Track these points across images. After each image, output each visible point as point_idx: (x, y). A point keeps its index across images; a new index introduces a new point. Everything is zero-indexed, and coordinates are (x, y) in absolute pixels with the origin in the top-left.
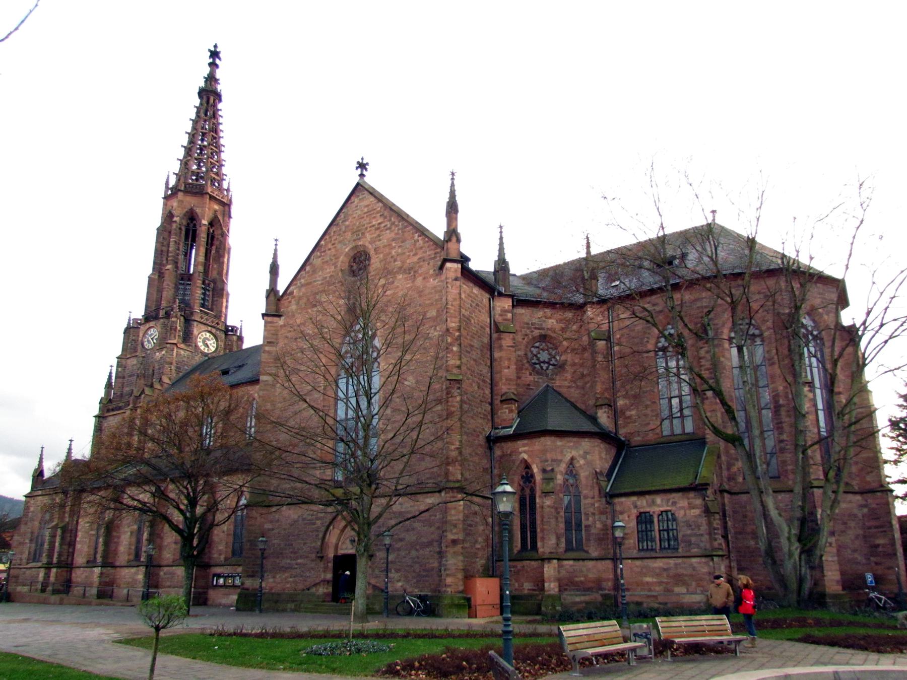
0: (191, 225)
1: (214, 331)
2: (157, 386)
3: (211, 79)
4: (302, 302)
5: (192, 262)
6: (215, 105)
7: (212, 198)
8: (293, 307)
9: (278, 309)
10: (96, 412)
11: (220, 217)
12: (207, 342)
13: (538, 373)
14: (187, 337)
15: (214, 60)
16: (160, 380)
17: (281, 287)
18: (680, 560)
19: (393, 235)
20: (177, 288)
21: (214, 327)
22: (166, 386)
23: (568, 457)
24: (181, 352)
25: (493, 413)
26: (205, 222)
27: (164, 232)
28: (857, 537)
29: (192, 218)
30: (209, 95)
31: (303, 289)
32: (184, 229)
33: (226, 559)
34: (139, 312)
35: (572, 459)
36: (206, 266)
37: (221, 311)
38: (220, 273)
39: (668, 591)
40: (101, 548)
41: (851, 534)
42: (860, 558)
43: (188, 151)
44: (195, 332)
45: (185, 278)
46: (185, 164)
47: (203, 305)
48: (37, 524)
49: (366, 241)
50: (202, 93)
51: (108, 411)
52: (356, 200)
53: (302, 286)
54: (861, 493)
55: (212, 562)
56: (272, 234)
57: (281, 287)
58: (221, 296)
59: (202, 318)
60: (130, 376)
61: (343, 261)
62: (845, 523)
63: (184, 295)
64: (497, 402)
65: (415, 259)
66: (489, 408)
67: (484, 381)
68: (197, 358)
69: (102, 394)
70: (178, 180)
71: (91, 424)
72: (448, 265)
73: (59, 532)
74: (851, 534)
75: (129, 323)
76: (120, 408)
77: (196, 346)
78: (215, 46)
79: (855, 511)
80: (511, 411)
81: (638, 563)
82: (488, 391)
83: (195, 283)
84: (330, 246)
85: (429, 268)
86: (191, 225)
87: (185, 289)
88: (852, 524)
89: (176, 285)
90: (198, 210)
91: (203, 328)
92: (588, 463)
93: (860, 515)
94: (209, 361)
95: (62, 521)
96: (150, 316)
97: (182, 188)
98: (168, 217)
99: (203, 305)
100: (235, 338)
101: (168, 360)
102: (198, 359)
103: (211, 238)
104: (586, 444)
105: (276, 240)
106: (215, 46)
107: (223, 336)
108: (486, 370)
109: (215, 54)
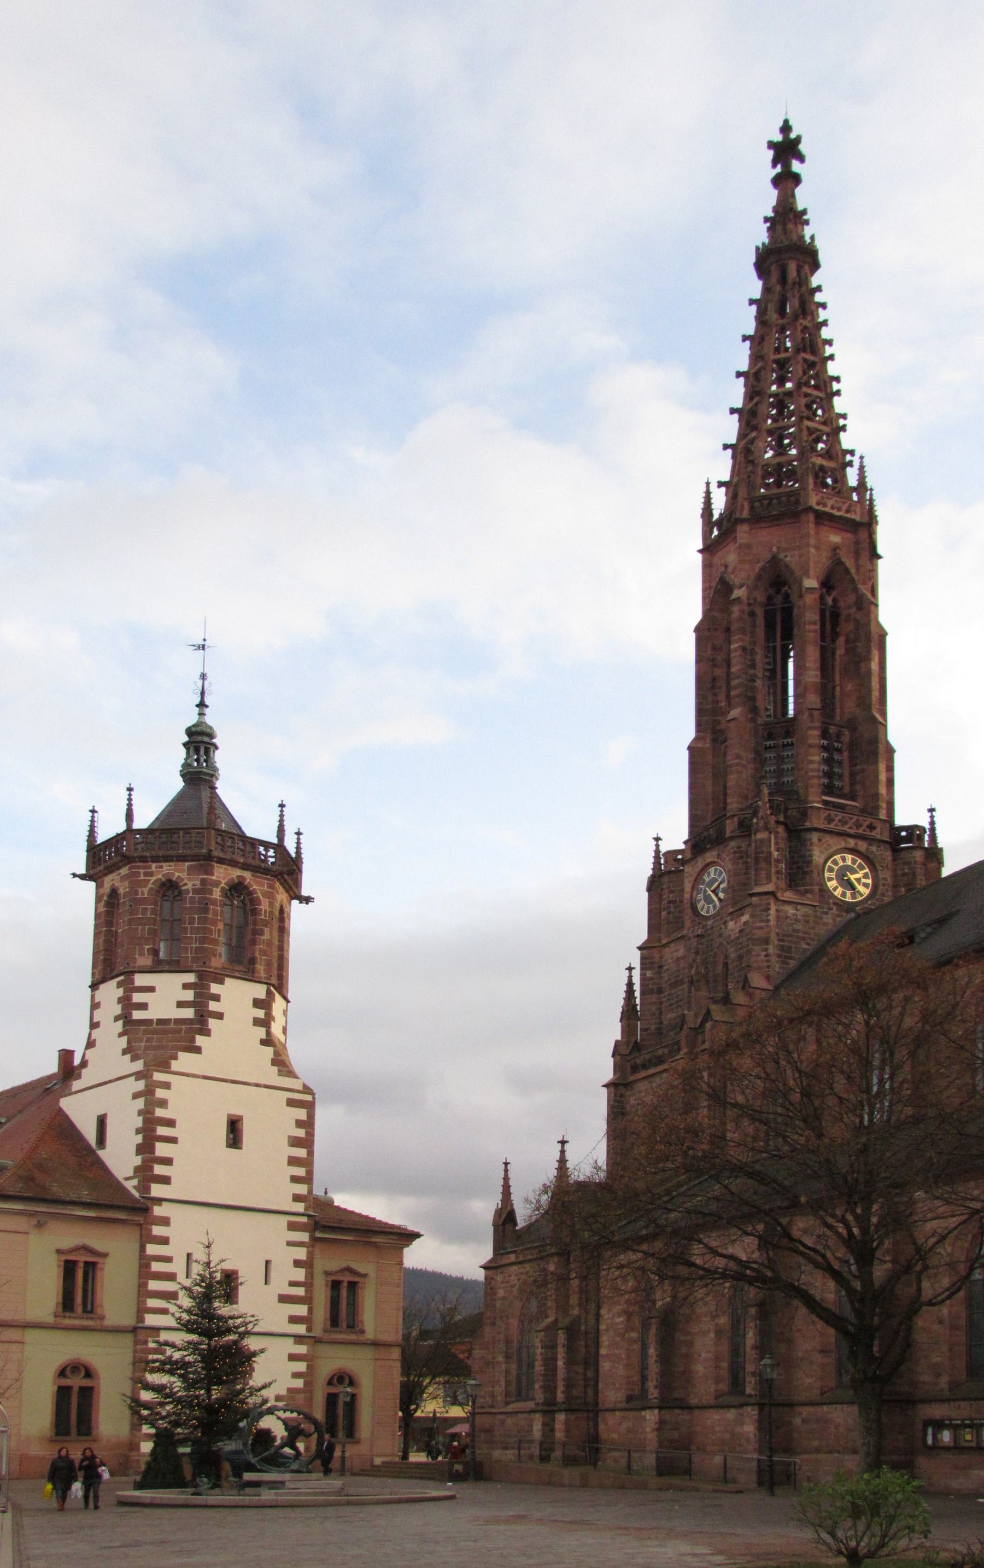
0: (779, 599)
1: (862, 846)
2: (739, 998)
3: (786, 217)
6: (803, 281)
10: (608, 1074)
11: (849, 563)
12: (849, 878)
14: (800, 873)
15: (787, 166)
21: (863, 838)
24: (790, 910)
29: (777, 580)
30: (787, 260)
32: (759, 612)
33: (954, 1385)
34: (676, 836)
37: (876, 796)
40: (654, 1368)
44: (817, 856)
45: (779, 731)
46: (742, 452)
47: (829, 789)
48: (514, 1322)
50: (766, 261)
51: (635, 1069)
60: (675, 985)
68: (828, 919)
69: (615, 1032)
73: (561, 1337)
77: (824, 892)
87: (780, 759)
89: (757, 753)
90: (791, 559)
94: (858, 919)
99: (829, 789)
102: (831, 921)
103: (831, 620)
107: (888, 855)
109: (786, 150)
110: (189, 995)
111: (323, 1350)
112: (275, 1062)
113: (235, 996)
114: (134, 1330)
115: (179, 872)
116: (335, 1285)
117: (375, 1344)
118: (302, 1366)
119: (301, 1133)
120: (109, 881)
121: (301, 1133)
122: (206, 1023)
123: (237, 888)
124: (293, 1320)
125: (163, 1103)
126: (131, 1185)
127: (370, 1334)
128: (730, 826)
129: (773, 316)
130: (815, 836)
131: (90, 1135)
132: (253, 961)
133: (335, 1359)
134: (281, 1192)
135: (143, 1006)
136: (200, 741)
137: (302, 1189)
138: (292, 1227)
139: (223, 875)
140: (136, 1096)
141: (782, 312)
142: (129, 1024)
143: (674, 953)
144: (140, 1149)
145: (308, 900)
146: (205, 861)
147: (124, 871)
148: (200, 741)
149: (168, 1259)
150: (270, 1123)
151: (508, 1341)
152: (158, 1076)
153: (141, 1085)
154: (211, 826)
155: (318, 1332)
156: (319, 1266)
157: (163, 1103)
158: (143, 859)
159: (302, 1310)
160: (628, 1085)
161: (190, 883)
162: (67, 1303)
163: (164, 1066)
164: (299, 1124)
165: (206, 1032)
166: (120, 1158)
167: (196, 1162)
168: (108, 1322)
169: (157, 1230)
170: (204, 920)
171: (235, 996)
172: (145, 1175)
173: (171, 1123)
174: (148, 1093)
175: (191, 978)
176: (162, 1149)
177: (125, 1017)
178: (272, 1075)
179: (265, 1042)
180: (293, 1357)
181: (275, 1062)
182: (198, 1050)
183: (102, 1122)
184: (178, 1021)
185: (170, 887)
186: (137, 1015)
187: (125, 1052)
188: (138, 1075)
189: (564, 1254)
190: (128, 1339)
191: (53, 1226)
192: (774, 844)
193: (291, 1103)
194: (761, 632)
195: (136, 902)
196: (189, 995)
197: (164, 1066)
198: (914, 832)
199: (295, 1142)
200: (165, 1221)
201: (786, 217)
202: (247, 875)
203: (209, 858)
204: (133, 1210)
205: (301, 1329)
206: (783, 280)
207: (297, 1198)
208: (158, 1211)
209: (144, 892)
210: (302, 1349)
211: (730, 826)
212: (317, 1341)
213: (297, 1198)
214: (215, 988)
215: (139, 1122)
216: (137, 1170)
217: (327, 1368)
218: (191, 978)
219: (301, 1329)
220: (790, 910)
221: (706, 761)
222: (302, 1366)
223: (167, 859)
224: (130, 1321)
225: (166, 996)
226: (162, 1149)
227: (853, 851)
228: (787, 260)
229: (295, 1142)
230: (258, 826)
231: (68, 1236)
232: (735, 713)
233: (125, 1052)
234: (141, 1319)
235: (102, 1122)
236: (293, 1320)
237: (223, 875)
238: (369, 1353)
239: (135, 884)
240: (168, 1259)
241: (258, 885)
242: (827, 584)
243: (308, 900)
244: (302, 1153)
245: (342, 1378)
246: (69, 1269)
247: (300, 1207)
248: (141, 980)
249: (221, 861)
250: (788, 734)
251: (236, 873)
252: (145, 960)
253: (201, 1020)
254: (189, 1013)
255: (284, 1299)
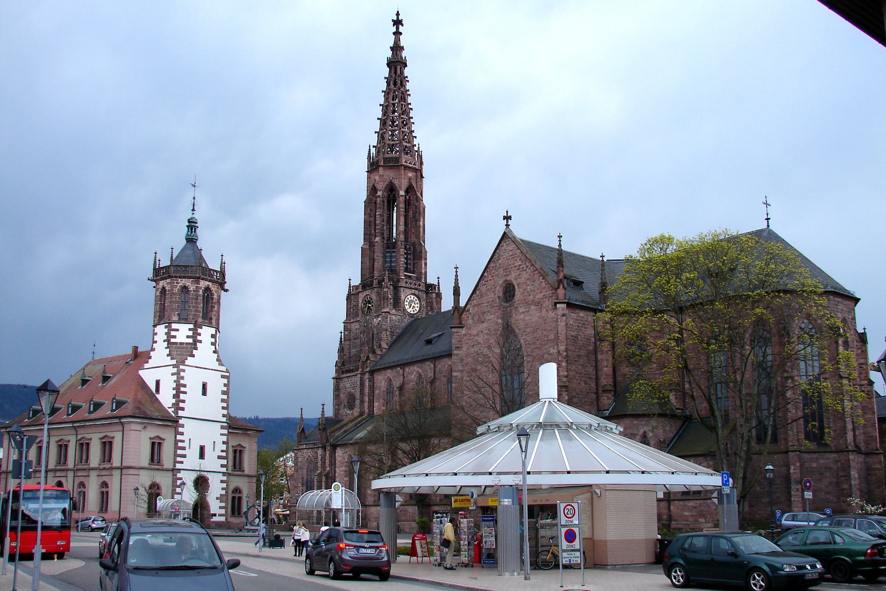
0: (392, 196)
1: (417, 292)
2: (378, 352)
3: (397, 48)
4: (476, 318)
5: (395, 223)
6: (402, 73)
7: (406, 167)
8: (470, 321)
9: (460, 323)
10: (334, 374)
11: (414, 184)
12: (412, 305)
13: (633, 365)
14: (397, 303)
15: (397, 28)
16: (380, 346)
17: (462, 303)
18: (702, 502)
19: (527, 276)
20: (385, 257)
21: (415, 289)
22: (384, 350)
23: (642, 431)
24: (395, 317)
25: (598, 399)
26: (402, 193)
27: (370, 204)
28: (831, 483)
29: (392, 189)
30: (396, 64)
31: (476, 309)
32: (386, 201)
33: (440, 500)
34: (357, 281)
35: (645, 432)
36: (406, 232)
37: (421, 273)
38: (418, 236)
39: (696, 521)
40: (139, 420)
41: (826, 482)
42: (831, 498)
43: (383, 122)
44: (403, 297)
45: (390, 245)
46: (381, 136)
47: (406, 270)
48: (305, 471)
49: (511, 278)
50: (390, 64)
51: (343, 373)
52: (505, 245)
53: (475, 305)
54: (837, 452)
55: (432, 503)
56: (455, 252)
57: (462, 303)
58: (420, 258)
59: (406, 283)
60: (355, 339)
61: (499, 291)
62: (821, 474)
63: (391, 262)
64: (600, 392)
65: (541, 296)
66: (594, 396)
67: (590, 378)
68: (405, 321)
69: (336, 358)
70: (378, 152)
71: (331, 384)
72: (558, 306)
73: (324, 479)
74: (826, 482)
75: (350, 289)
76: (352, 371)
77: (404, 310)
78: (398, 14)
79: (832, 465)
80: (608, 398)
81: (681, 503)
82: (593, 385)
83: (399, 252)
84: (490, 278)
85: (548, 304)
86: (392, 196)
87: (391, 257)
88: (828, 474)
89: (384, 254)
90: (396, 182)
91: (408, 291)
92: (655, 435)
93: (835, 467)
94: (415, 320)
95: (325, 470)
96: (366, 284)
97: (382, 164)
98: (372, 190)
99: (406, 270)
100: (434, 295)
101: (384, 327)
102: (407, 320)
103: (408, 203)
104: (653, 422)
105: (456, 268)
106: (398, 14)
107: (425, 295)
108: (591, 370)
109: (398, 23)
110: (191, 333)
111: (232, 478)
112: (217, 360)
113: (206, 332)
114: (173, 470)
115: (188, 282)
116: (235, 451)
117: (248, 476)
118: (224, 485)
119: (225, 389)
120: (162, 283)
121: (225, 389)
122: (196, 345)
123: (207, 289)
124: (222, 466)
125: (183, 378)
126: (171, 411)
127: (246, 472)
128: (375, 282)
129: (392, 86)
130: (402, 289)
131: (153, 388)
132: (211, 319)
133: (237, 482)
134: (218, 414)
135: (175, 337)
136: (192, 225)
137: (225, 412)
138: (222, 427)
139: (203, 284)
140: (173, 374)
141: (395, 84)
142: (170, 344)
143: (355, 326)
144: (175, 396)
145: (226, 291)
146: (197, 279)
147: (168, 280)
148: (192, 225)
149: (183, 441)
150: (216, 385)
151: (303, 478)
152: (182, 367)
153: (175, 370)
154: (200, 265)
155: (230, 471)
156: (231, 444)
157: (183, 378)
158: (176, 277)
159: (224, 462)
160: (341, 379)
161: (192, 288)
162: (152, 459)
163: (183, 363)
164: (225, 385)
165: (196, 349)
166: (166, 398)
167: (193, 403)
168: (165, 467)
169: (180, 430)
170: (196, 303)
171: (206, 332)
172: (177, 407)
173: (185, 386)
174: (178, 373)
175: (192, 326)
176: (182, 397)
177: (168, 341)
178: (216, 365)
179: (214, 352)
180: (222, 482)
181: (217, 360)
182: (193, 356)
183: (158, 383)
184: (187, 344)
185: (185, 289)
186: (173, 340)
187: (168, 355)
188: (174, 366)
189: (324, 448)
190: (170, 474)
191: (149, 428)
192: (389, 293)
193: (223, 377)
194: (386, 208)
195: (173, 294)
196: (191, 333)
197: (183, 363)
198: (431, 286)
199: (224, 393)
200: (183, 426)
201: (397, 48)
202: (210, 284)
203: (199, 278)
204: (173, 422)
205: (224, 470)
206: (396, 73)
207: (224, 416)
208: (181, 422)
209: (176, 290)
210: (225, 478)
211: (375, 282)
212: (229, 474)
213: (224, 416)
214: (199, 330)
215: (174, 385)
216: (173, 404)
217: (232, 487)
218: (192, 326)
219: (224, 470)
220: (394, 318)
221: (368, 254)
222: (224, 485)
223: (184, 277)
224: (171, 467)
225: (182, 333)
226: (182, 397)
227: (413, 294)
228: (396, 64)
229: (224, 393)
230: (213, 264)
231: (152, 432)
232: (377, 239)
233: (168, 355)
234: (175, 466)
235: (158, 383)
236: (222, 466)
237: (203, 284)
238: (246, 479)
239: (173, 287)
240: (183, 441)
241: (214, 288)
242: (407, 192)
243: (226, 291)
244: (225, 397)
245: (237, 490)
246: (153, 444)
247: (224, 419)
248: (174, 326)
249: (203, 279)
250: (394, 247)
251: (207, 283)
252: (176, 318)
253: (194, 345)
254: (190, 341)
255: (219, 457)
